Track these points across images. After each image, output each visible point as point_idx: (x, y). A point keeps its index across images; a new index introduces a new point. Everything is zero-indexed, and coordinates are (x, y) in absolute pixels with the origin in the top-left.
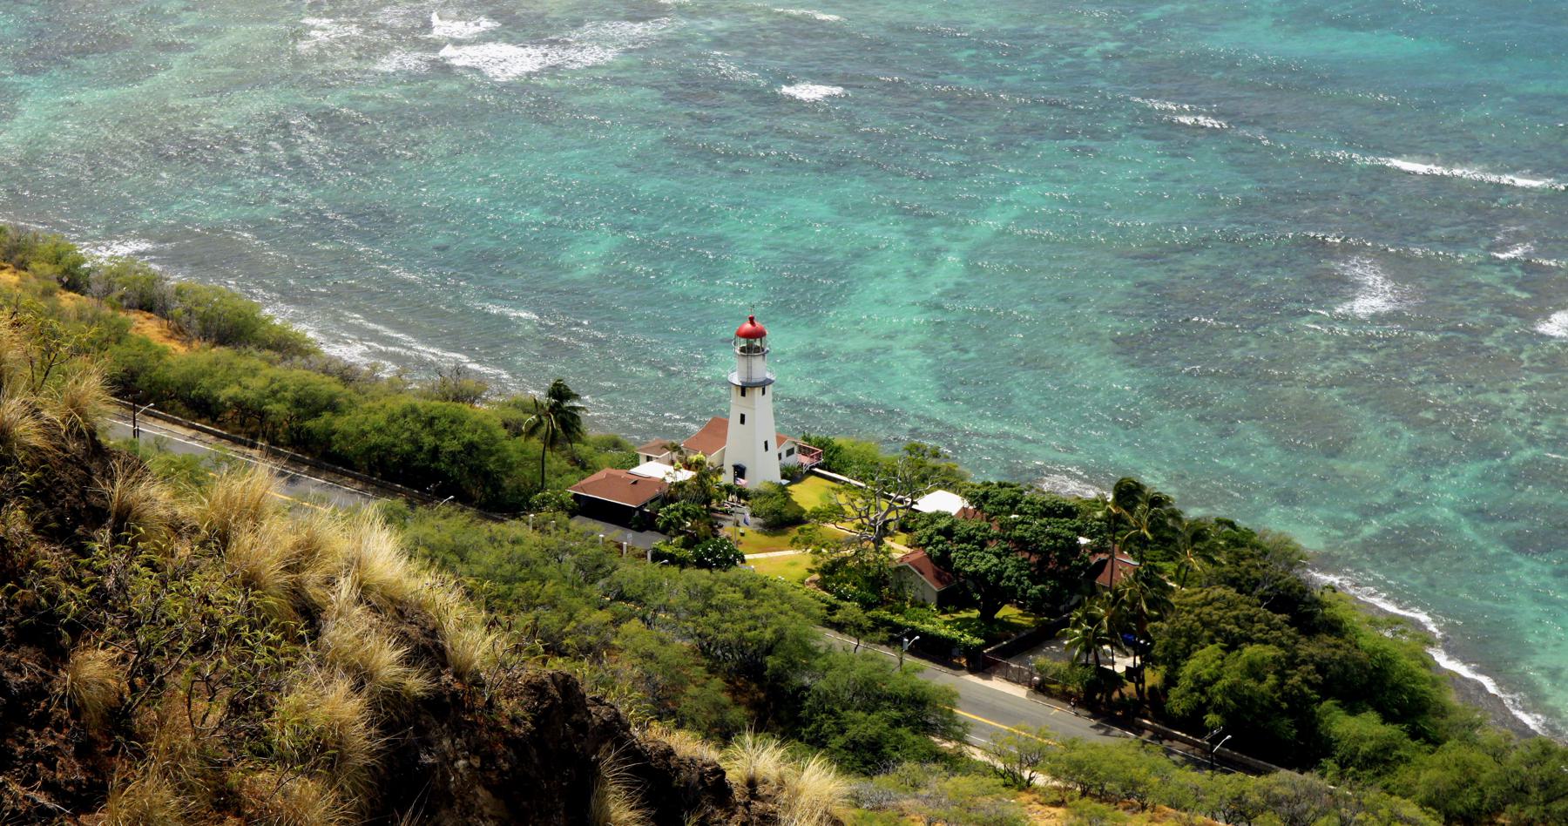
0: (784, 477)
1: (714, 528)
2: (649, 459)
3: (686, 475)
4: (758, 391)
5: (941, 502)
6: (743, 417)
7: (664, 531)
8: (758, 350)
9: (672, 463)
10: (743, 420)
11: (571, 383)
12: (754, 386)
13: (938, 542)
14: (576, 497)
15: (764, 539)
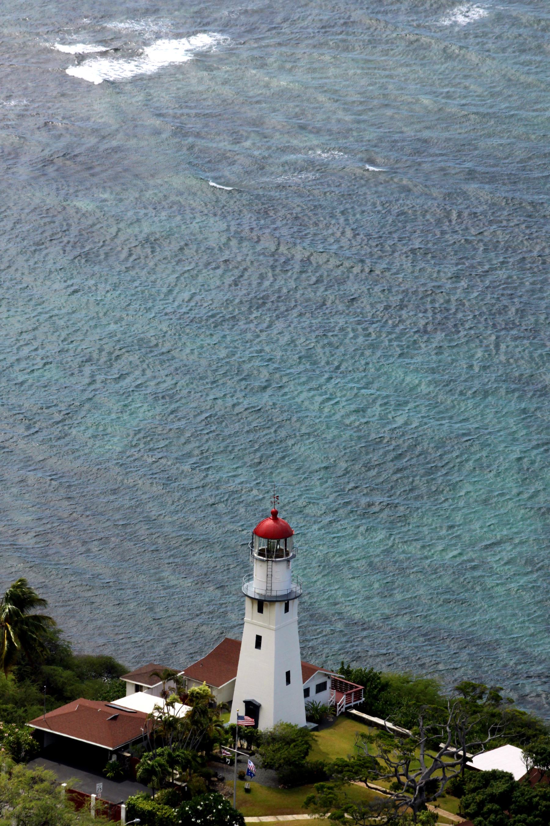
0: (309, 719)
1: (212, 782)
2: (138, 689)
3: (181, 710)
4: (279, 608)
5: (508, 760)
6: (288, 681)
7: (145, 781)
8: (280, 554)
9: (164, 695)
10: (258, 645)
11: (34, 582)
12: (273, 601)
13: (490, 811)
14: (37, 734)
15: (274, 797)
